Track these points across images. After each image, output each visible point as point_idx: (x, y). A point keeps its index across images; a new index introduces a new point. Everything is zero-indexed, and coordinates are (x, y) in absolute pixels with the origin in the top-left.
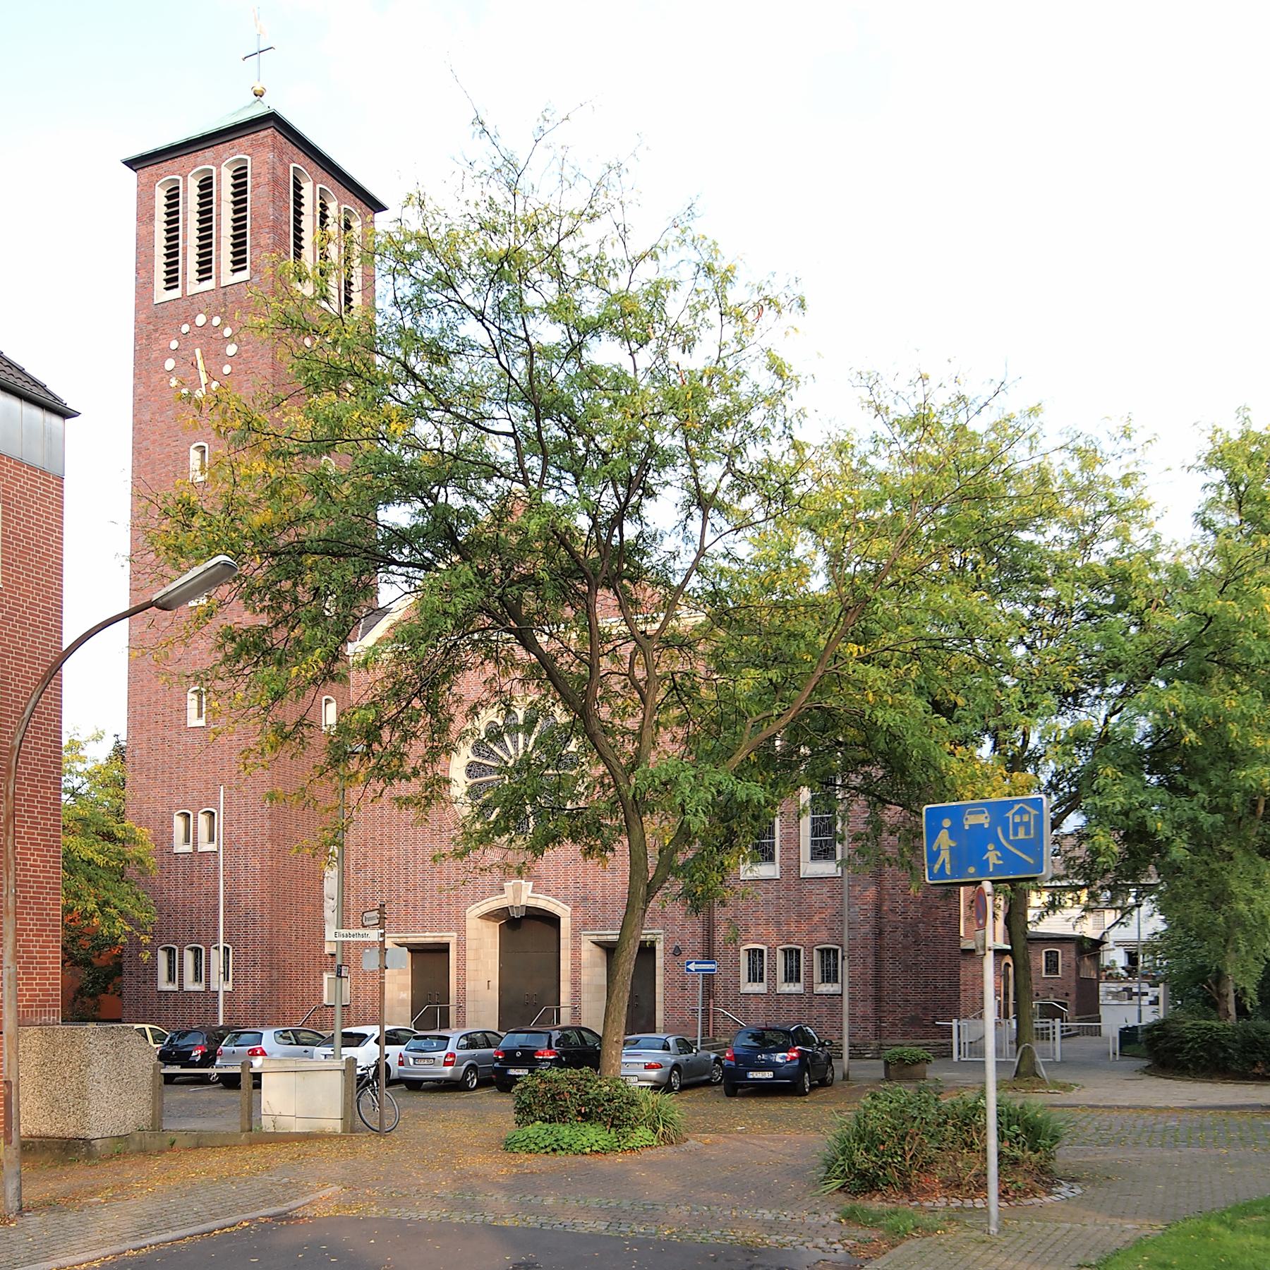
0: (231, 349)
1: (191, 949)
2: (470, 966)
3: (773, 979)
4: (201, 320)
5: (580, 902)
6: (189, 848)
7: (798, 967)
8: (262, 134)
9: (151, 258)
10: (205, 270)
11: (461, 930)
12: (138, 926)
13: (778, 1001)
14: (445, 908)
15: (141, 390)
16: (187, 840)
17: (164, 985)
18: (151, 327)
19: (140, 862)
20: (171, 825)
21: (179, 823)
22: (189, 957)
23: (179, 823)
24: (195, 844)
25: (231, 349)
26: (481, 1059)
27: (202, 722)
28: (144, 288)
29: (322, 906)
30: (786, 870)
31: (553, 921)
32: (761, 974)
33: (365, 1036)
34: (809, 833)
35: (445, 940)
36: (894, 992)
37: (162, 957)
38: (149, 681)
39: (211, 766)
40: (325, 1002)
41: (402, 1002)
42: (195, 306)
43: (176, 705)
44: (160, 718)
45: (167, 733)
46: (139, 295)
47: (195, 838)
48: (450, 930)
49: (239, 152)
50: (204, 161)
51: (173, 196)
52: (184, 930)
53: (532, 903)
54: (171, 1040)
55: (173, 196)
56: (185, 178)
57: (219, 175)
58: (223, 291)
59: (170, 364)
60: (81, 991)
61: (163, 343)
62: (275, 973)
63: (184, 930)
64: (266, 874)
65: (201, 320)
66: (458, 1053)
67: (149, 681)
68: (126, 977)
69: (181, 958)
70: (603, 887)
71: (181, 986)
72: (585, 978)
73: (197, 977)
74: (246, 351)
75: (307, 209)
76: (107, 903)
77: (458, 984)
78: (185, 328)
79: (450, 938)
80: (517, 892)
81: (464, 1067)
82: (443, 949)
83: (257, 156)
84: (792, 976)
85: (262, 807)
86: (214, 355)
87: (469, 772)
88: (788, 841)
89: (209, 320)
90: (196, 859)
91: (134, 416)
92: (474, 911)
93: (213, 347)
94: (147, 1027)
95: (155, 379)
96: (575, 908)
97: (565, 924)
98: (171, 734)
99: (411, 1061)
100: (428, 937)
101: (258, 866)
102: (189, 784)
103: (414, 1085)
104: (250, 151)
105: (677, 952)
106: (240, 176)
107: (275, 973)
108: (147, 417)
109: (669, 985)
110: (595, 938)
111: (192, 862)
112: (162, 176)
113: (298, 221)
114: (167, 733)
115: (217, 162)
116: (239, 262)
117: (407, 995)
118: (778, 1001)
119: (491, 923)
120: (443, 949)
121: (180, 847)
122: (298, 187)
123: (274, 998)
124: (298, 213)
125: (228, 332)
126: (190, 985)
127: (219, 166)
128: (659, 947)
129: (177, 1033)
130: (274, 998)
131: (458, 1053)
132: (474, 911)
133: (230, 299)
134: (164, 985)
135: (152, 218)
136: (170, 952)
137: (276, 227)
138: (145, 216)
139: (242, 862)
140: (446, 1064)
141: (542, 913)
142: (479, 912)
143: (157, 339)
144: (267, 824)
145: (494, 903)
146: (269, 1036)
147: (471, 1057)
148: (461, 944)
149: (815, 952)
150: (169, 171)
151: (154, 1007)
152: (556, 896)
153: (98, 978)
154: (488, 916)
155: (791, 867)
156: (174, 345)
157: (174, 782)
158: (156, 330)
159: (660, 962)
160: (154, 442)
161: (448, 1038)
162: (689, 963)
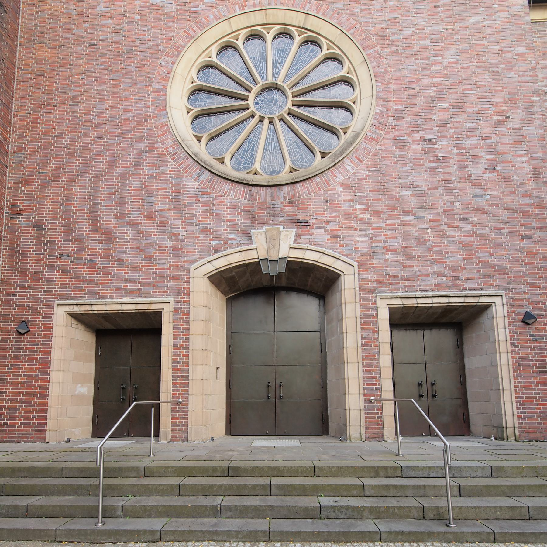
11: (183, 295)
53: (296, 255)
77: (175, 369)
80: (273, 241)
105: (528, 319)
128: (499, 309)
148: (183, 315)
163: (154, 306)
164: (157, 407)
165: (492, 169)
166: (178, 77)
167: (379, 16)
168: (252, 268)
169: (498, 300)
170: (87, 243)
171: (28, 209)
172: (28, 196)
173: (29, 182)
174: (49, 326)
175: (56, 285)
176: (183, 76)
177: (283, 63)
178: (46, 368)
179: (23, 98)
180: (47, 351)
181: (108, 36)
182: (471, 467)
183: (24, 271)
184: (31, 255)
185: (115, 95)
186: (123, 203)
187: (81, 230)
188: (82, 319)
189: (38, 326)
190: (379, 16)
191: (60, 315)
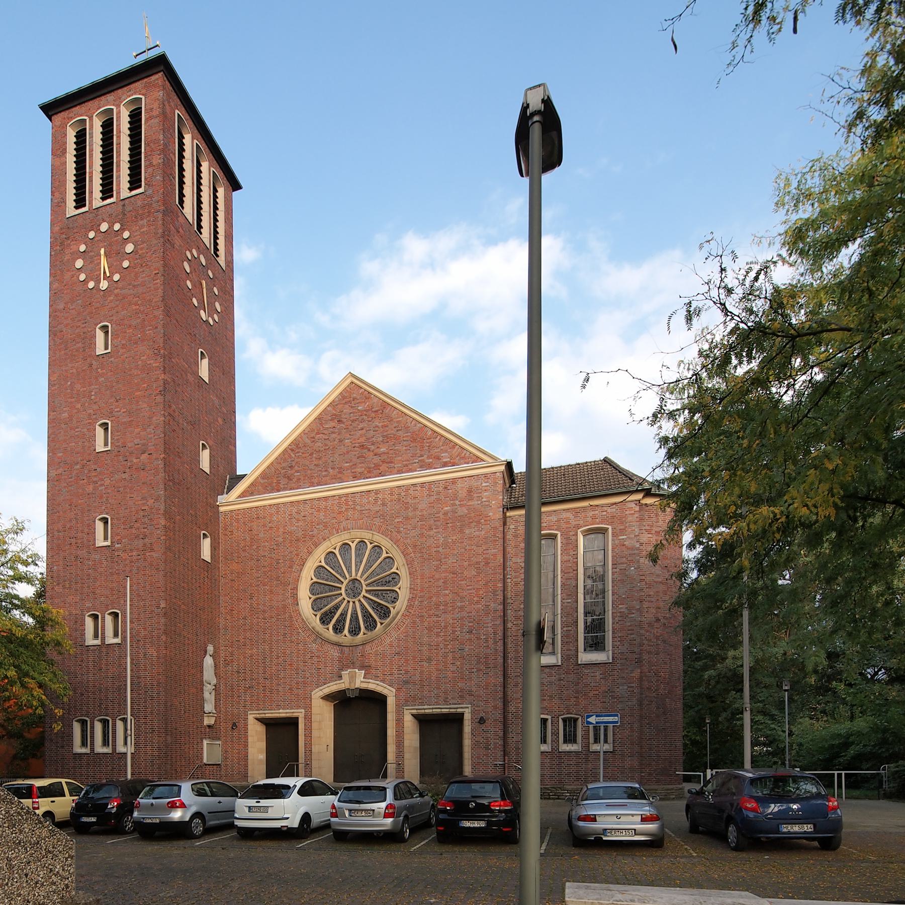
0: (129, 248)
1: (100, 721)
2: (315, 733)
3: (555, 741)
4: (104, 227)
5: (402, 685)
6: (98, 642)
7: (575, 731)
8: (153, 78)
9: (64, 183)
10: (107, 191)
11: (308, 708)
12: (54, 697)
13: (560, 758)
14: (296, 691)
15: (56, 285)
16: (96, 636)
17: (78, 749)
18: (64, 236)
19: (58, 644)
20: (83, 624)
21: (77, 728)
22: (98, 727)
23: (89, 623)
24: (103, 638)
25: (129, 248)
26: (410, 808)
27: (108, 543)
28: (58, 205)
29: (202, 690)
30: (566, 658)
31: (379, 700)
32: (575, 735)
33: (288, 787)
34: (582, 631)
35: (295, 715)
36: (650, 749)
37: (77, 728)
38: (65, 512)
39: (115, 576)
40: (205, 761)
41: (261, 760)
42: (100, 217)
43: (86, 530)
44: (74, 541)
45: (79, 553)
46: (53, 212)
47: (103, 633)
48: (299, 707)
49: (135, 93)
50: (106, 103)
51: (81, 137)
52: (96, 702)
53: (364, 686)
54: (87, 793)
55: (81, 137)
56: (91, 118)
57: (119, 113)
58: (122, 203)
59: (79, 263)
60: (15, 757)
61: (74, 248)
62: (169, 738)
63: (96, 702)
64: (162, 660)
65: (104, 227)
66: (397, 803)
67: (65, 512)
68: (47, 744)
69: (92, 727)
70: (422, 673)
71: (92, 749)
72: (407, 743)
73: (105, 743)
74: (142, 249)
75: (187, 154)
76: (27, 675)
77: (305, 747)
78: (92, 235)
79: (300, 713)
80: (353, 677)
81: (401, 818)
82: (293, 723)
83: (149, 95)
84: (570, 738)
85: (158, 607)
86: (115, 255)
87: (312, 591)
88: (568, 636)
89: (111, 227)
90: (104, 650)
91: (51, 306)
92: (318, 694)
93: (114, 248)
94: (63, 781)
95: (67, 276)
96: (398, 690)
97: (391, 702)
98: (83, 553)
99: (347, 813)
100: (282, 713)
101: (155, 654)
102: (98, 591)
103: (343, 837)
104: (144, 91)
105: (482, 721)
106: (135, 117)
107: (169, 738)
108: (61, 306)
109: (475, 745)
110: (414, 712)
111: (100, 652)
112: (72, 118)
113: (181, 163)
114: (79, 553)
115: (117, 103)
116: (135, 183)
117: (262, 756)
118: (560, 758)
119: (328, 703)
120: (293, 723)
121: (90, 641)
122: (181, 137)
123: (169, 758)
124: (181, 157)
125: (126, 235)
126: (99, 749)
127: (118, 106)
128: (467, 716)
129: (92, 786)
130: (169, 758)
131: (397, 803)
132: (318, 694)
133: (128, 208)
134: (78, 749)
135: (64, 151)
136: (83, 723)
137: (165, 151)
138: (58, 150)
139: (142, 651)
140: (386, 816)
141: (272, 722)
142: (321, 694)
143: (69, 245)
144: (163, 620)
145: (333, 687)
146: (186, 787)
147: (405, 808)
148: (308, 718)
149: (561, 721)
150: (78, 114)
151: (68, 764)
152: (383, 681)
153: (27, 747)
154: (328, 698)
155: (570, 656)
156: (83, 248)
157: (86, 590)
158: (68, 238)
159: (467, 728)
160: (67, 325)
161: (384, 789)
162: (589, 717)
163: (459, 710)
164: (297, 766)
165: (470, 632)
166: (303, 579)
167: (413, 533)
168: (342, 692)
169: (466, 710)
170: (262, 681)
171: (232, 661)
172: (232, 654)
173: (232, 647)
174: (246, 725)
175: (248, 703)
176: (307, 576)
177: (361, 562)
178: (246, 746)
179: (225, 595)
180: (246, 737)
181: (266, 554)
182: (618, 884)
183: (232, 696)
184: (236, 688)
185: (271, 591)
186: (278, 658)
187: (258, 673)
188: (328, 698)
189: (241, 725)
190: (413, 533)
191: (251, 718)
